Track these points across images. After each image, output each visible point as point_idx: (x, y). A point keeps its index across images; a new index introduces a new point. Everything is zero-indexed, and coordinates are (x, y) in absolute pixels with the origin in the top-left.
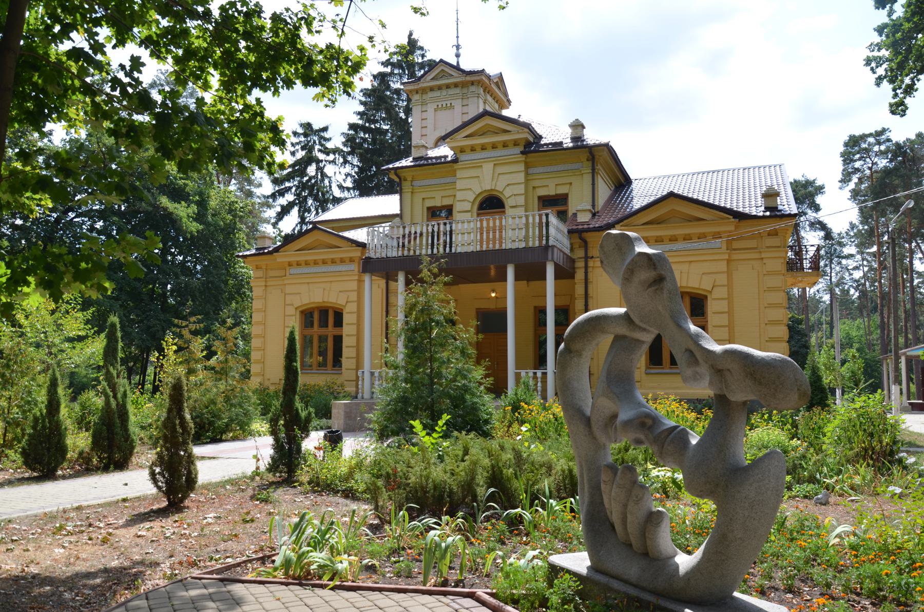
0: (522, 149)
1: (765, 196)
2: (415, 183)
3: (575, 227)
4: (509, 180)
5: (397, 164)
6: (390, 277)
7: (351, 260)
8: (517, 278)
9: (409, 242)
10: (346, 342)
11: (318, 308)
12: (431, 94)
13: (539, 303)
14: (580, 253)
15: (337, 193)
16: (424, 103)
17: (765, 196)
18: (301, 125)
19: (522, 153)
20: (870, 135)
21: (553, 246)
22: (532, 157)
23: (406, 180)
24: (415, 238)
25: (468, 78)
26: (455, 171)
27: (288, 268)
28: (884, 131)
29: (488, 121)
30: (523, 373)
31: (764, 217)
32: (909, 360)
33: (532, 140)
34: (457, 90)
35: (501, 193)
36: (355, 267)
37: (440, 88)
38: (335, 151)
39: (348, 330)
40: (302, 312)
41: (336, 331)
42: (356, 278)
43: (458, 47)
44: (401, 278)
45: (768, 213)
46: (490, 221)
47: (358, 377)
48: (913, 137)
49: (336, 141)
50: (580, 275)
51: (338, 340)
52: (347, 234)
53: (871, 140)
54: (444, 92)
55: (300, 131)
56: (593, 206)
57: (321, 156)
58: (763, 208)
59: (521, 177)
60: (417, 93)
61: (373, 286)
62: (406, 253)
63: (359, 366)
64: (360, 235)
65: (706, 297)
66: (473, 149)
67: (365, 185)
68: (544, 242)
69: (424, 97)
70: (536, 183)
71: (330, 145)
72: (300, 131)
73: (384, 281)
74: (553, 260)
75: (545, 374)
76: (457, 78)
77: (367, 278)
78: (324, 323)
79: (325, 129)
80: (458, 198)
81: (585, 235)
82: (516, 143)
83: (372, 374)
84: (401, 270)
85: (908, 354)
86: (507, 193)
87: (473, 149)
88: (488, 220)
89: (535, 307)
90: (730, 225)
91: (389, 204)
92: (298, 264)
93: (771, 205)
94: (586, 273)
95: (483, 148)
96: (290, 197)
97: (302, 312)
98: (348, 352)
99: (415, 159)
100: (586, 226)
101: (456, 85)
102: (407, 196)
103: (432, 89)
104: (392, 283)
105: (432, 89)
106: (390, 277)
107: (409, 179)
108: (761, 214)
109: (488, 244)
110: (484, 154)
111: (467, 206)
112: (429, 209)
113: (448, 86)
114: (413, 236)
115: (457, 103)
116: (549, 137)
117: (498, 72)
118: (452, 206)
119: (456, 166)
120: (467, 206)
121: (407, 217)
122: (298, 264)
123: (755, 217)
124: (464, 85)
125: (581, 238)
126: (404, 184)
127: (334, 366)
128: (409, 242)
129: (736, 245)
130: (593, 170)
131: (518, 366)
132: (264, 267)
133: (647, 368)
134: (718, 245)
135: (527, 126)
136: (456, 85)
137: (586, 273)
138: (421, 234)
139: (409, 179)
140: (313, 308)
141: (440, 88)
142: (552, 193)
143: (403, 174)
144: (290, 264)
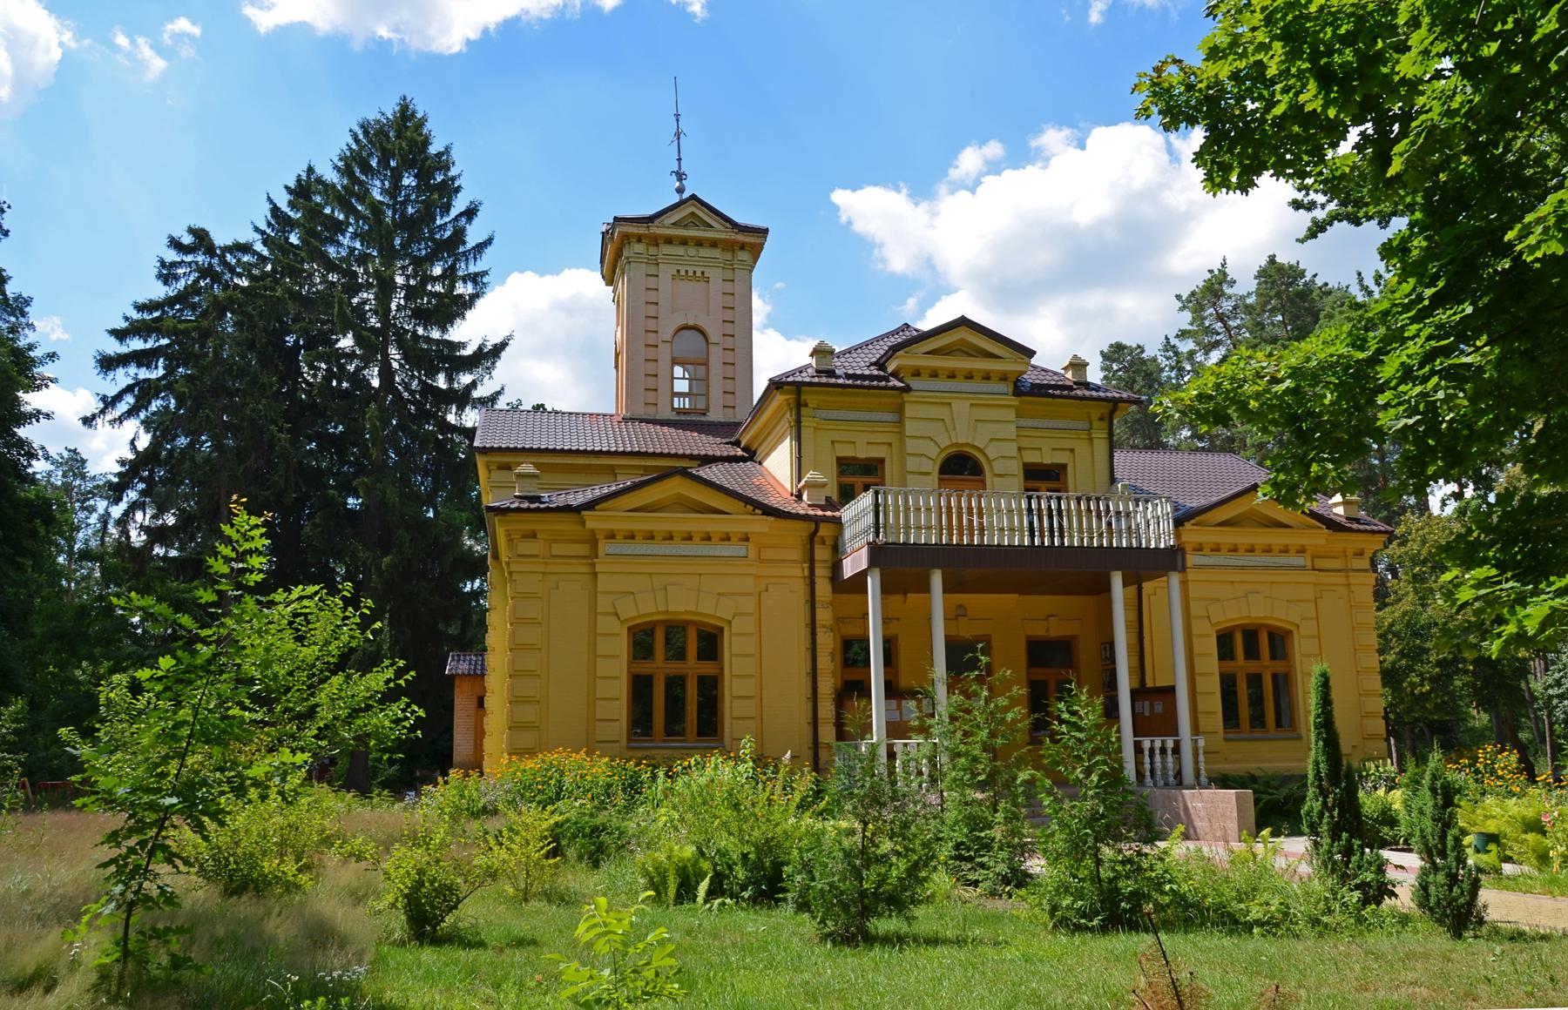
4: (999, 437)
8: (946, 590)
12: (666, 249)
13: (852, 631)
18: (191, 231)
25: (740, 237)
30: (1146, 743)
34: (716, 253)
37: (684, 242)
40: (1289, 633)
41: (707, 668)
43: (680, 176)
54: (692, 251)
55: (187, 240)
59: (1011, 431)
66: (934, 375)
72: (187, 240)
75: (1177, 744)
76: (719, 232)
78: (1252, 652)
82: (1004, 378)
84: (1117, 569)
86: (992, 452)
87: (934, 375)
89: (1074, 637)
101: (714, 244)
103: (669, 241)
105: (669, 241)
109: (950, 535)
113: (699, 243)
115: (715, 275)
119: (906, 397)
124: (730, 246)
127: (700, 733)
129: (767, 554)
130: (798, 422)
133: (629, 740)
134: (742, 552)
136: (714, 244)
141: (684, 242)
142: (862, 455)
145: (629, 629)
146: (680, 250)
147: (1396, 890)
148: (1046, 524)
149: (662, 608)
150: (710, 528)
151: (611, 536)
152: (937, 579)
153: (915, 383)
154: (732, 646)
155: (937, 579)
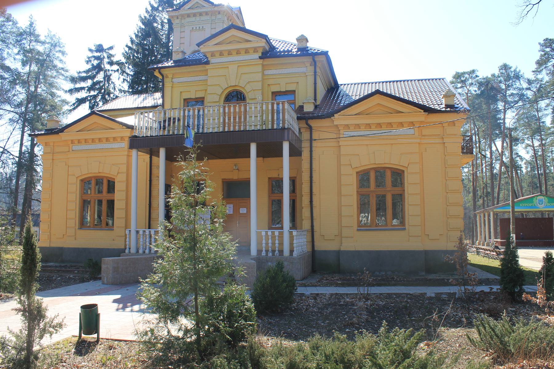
0: (260, 55)
1: (445, 96)
2: (174, 80)
3: (302, 115)
5: (160, 65)
6: (153, 153)
7: (122, 138)
9: (169, 125)
10: (118, 205)
11: (94, 177)
13: (274, 175)
14: (306, 135)
15: (117, 93)
16: (182, 26)
17: (445, 96)
19: (260, 58)
20: (467, 73)
21: (289, 129)
22: (268, 61)
23: (167, 77)
24: (174, 122)
26: (207, 70)
27: (71, 145)
28: (473, 71)
29: (233, 32)
31: (445, 112)
32: (496, 214)
33: (267, 48)
35: (243, 88)
36: (125, 144)
37: (195, 15)
38: (118, 63)
39: (118, 196)
41: (397, 190)
42: (126, 153)
44: (162, 152)
45: (449, 109)
46: (234, 108)
47: (126, 235)
48: (490, 76)
49: (119, 57)
50: (305, 154)
51: (111, 204)
52: (119, 119)
53: (467, 76)
56: (315, 100)
57: (108, 67)
58: (444, 106)
60: (178, 18)
61: (139, 159)
62: (166, 133)
63: (127, 226)
64: (130, 120)
65: (403, 171)
66: (221, 54)
67: (138, 86)
68: (281, 125)
69: (183, 21)
70: (271, 82)
71: (115, 59)
73: (149, 156)
74: (288, 140)
75: (281, 234)
77: (134, 152)
79: (111, 48)
80: (208, 92)
81: (162, 70)
82: (255, 50)
83: (137, 232)
84: (162, 147)
85: (495, 210)
87: (221, 54)
88: (235, 107)
90: (421, 116)
91: (155, 99)
92: (79, 141)
93: (450, 103)
94: (311, 151)
95: (230, 53)
96: (83, 94)
97: (82, 181)
98: (118, 212)
99: (175, 62)
100: (311, 115)
102: (167, 90)
103: (189, 16)
104: (154, 158)
105: (189, 16)
106: (153, 153)
107: (170, 76)
108: (444, 109)
109: (234, 126)
110: (230, 58)
111: (216, 98)
112: (185, 100)
114: (172, 120)
116: (280, 48)
117: (238, 6)
118: (204, 98)
120: (216, 98)
121: (167, 106)
122: (79, 141)
123: (440, 111)
125: (307, 124)
126: (166, 80)
128: (169, 125)
129: (425, 132)
131: (258, 227)
132: (52, 144)
135: (265, 37)
137: (311, 151)
138: (179, 120)
139: (170, 76)
140: (91, 177)
141: (195, 15)
143: (164, 72)
144: (72, 142)
145: (357, 173)
146: (193, 19)
147: (116, 305)
148: (196, 123)
149: (372, 162)
150: (114, 135)
151: (347, 126)
152: (253, 148)
153: (212, 60)
154: (409, 179)
155: (253, 148)
